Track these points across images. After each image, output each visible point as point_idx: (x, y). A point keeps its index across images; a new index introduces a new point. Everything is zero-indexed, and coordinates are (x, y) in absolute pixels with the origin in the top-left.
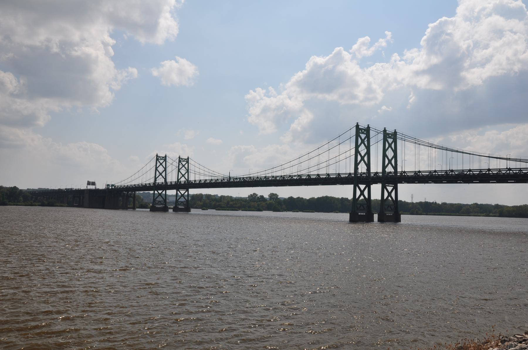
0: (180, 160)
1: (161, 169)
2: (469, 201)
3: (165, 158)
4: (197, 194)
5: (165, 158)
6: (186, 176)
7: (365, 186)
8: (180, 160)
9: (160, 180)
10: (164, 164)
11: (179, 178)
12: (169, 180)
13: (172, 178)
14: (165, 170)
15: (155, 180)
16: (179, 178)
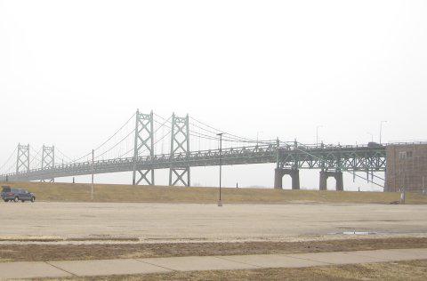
0: (175, 119)
1: (144, 135)
2: (244, 184)
3: (150, 117)
4: (158, 174)
5: (150, 117)
6: (185, 146)
7: (140, 184)
8: (175, 119)
9: (144, 153)
10: (149, 127)
11: (174, 149)
12: (158, 152)
13: (162, 148)
14: (151, 136)
15: (136, 152)
16: (174, 149)
